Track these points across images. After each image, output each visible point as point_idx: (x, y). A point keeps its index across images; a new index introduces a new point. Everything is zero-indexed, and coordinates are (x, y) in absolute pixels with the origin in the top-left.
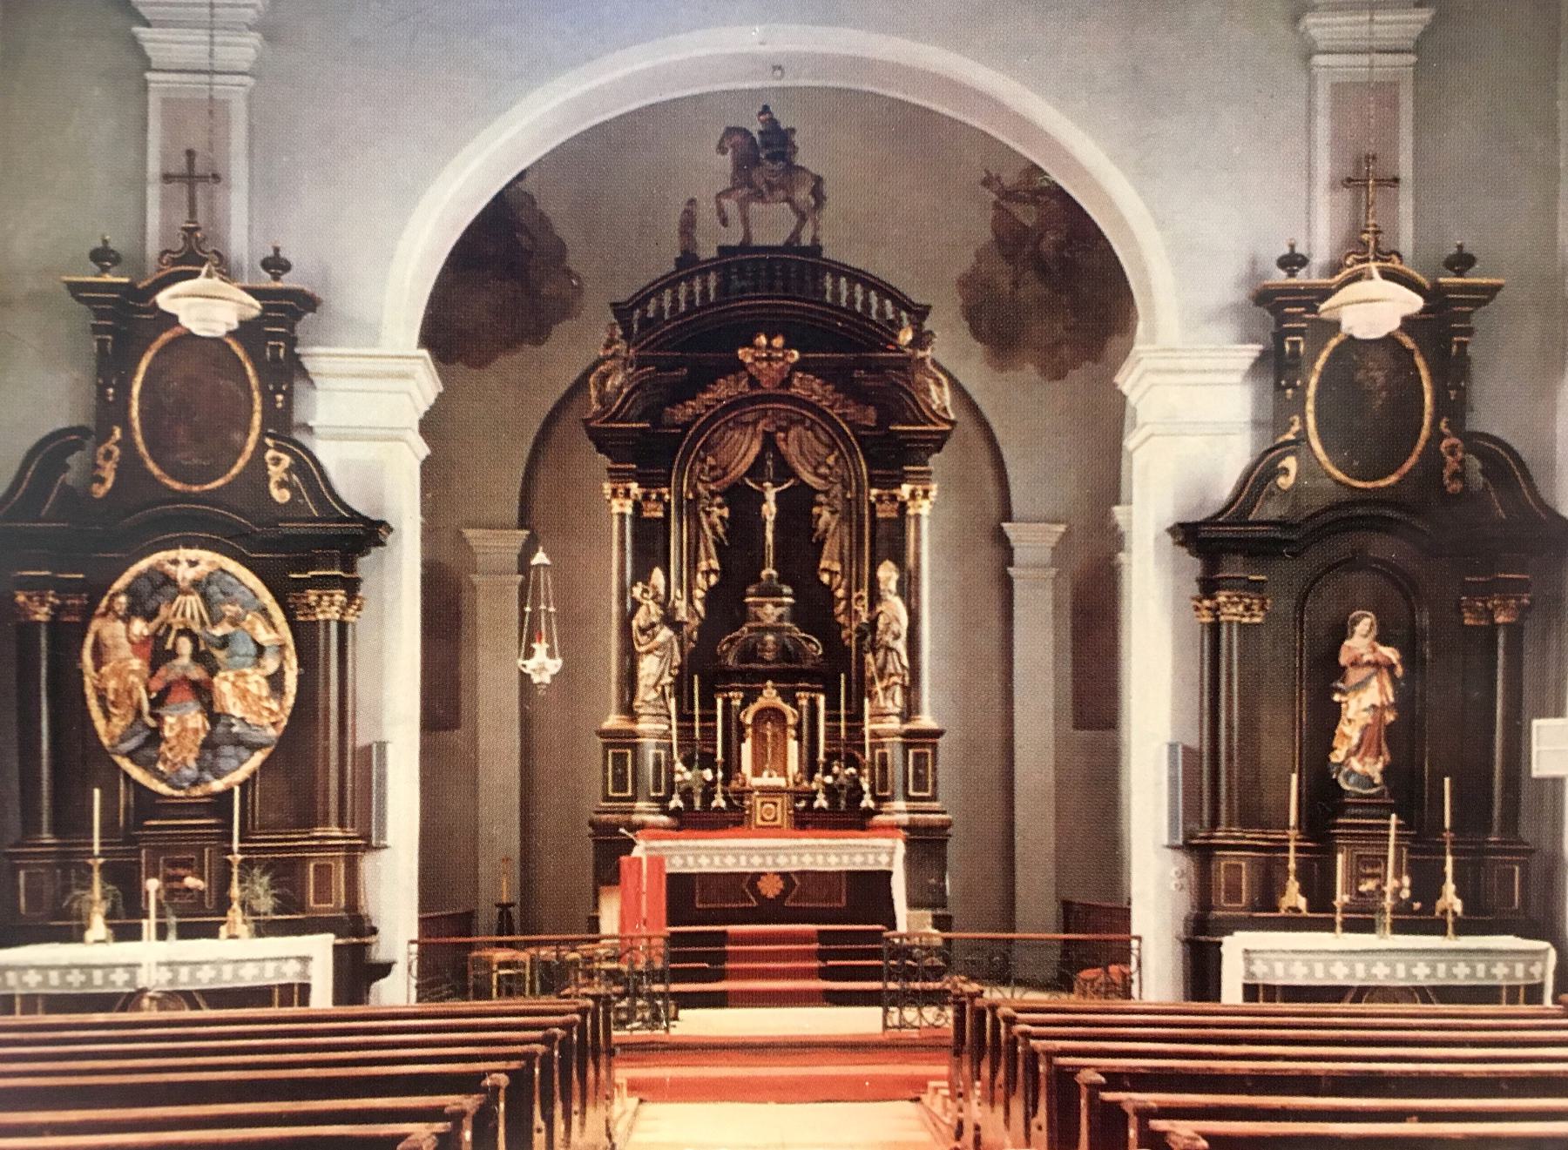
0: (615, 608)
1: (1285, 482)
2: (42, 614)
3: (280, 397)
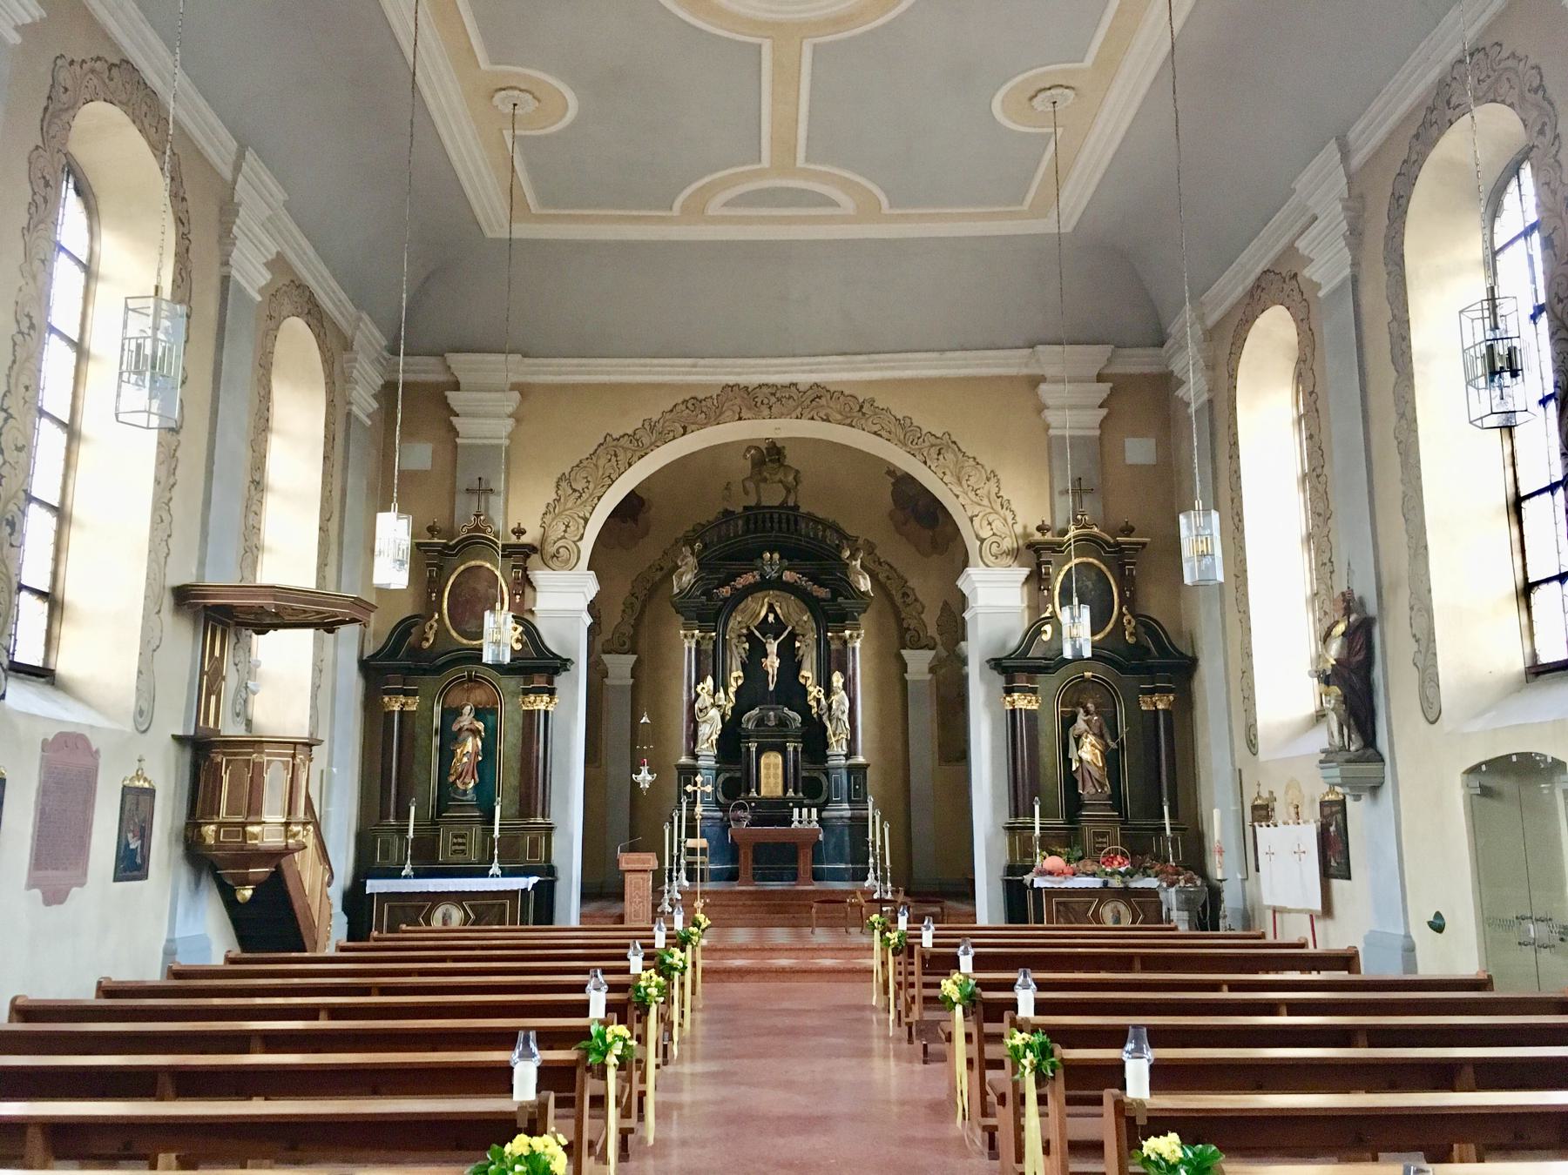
0: (685, 698)
1: (1046, 637)
2: (397, 708)
3: (518, 597)
